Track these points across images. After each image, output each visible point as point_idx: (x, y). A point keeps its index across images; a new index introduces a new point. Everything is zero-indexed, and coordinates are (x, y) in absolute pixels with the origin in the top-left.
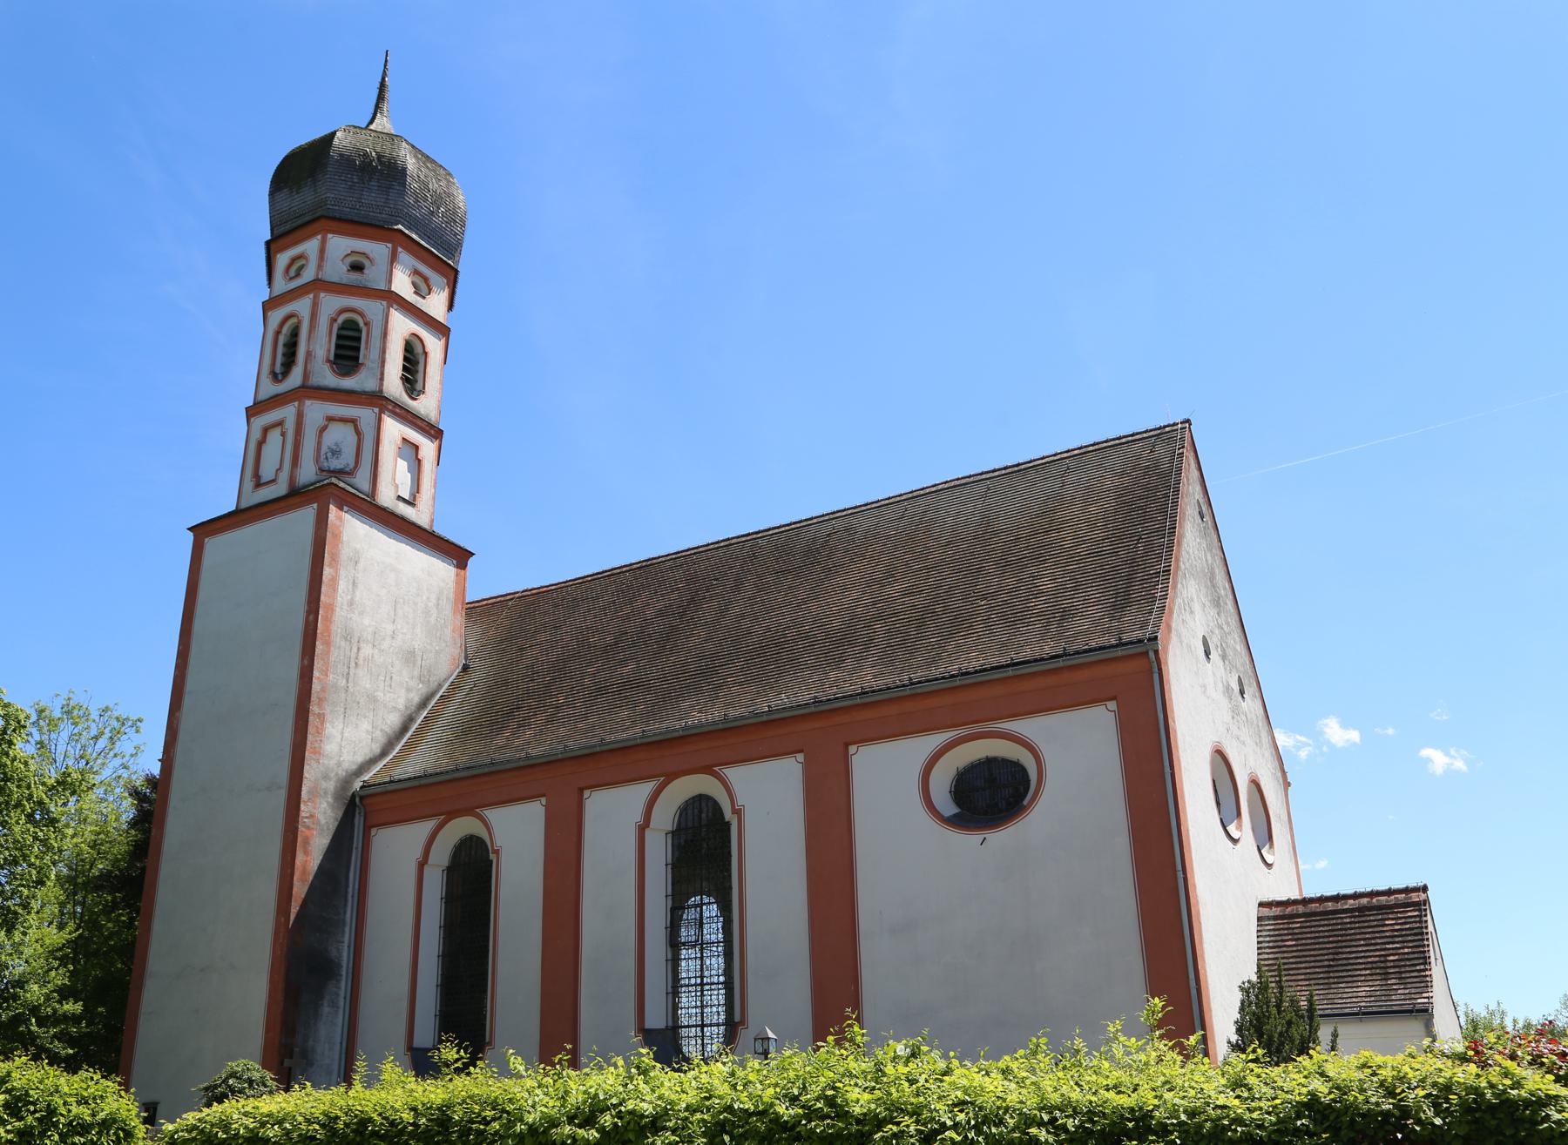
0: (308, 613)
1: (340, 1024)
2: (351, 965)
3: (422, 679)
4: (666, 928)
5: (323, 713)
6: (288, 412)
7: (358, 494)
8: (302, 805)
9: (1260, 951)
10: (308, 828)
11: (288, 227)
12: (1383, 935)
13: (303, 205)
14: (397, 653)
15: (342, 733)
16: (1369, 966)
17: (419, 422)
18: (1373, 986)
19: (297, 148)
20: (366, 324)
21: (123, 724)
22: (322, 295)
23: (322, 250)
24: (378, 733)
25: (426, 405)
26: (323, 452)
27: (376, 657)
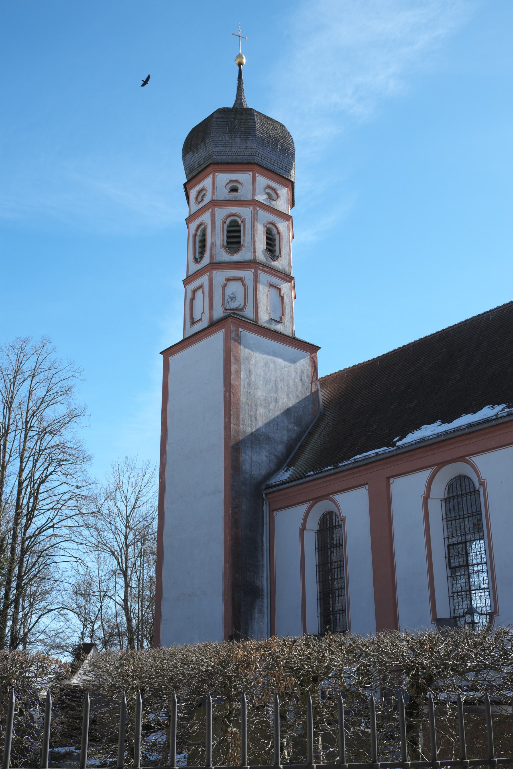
0: (225, 392)
1: (266, 623)
2: (269, 590)
4: (446, 558)
6: (204, 280)
11: (194, 173)
13: (201, 159)
20: (242, 222)
22: (216, 209)
24: (273, 457)
26: (226, 299)
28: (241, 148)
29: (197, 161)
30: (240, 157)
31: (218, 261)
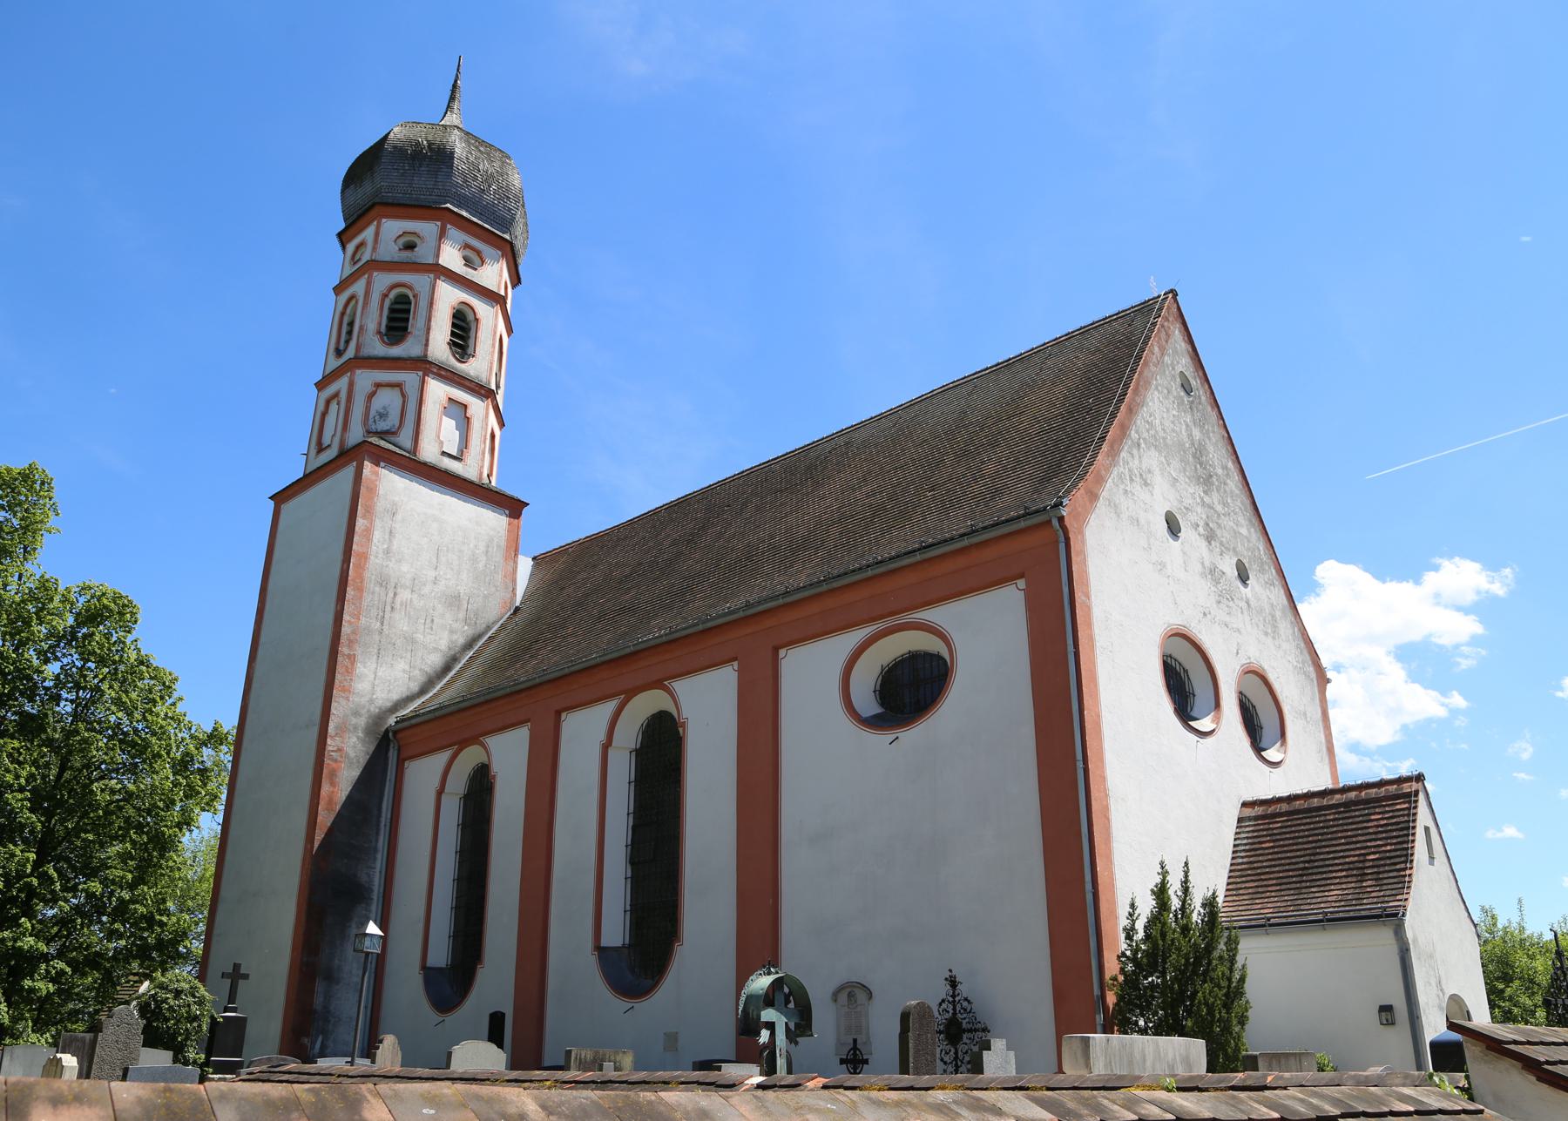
0: (344, 562)
3: (468, 621)
4: (627, 846)
5: (354, 655)
6: (342, 384)
9: (1235, 855)
10: (336, 761)
12: (1366, 831)
14: (439, 597)
15: (375, 673)
16: (1346, 867)
17: (467, 383)
18: (1345, 889)
20: (414, 296)
22: (375, 274)
24: (417, 672)
25: (478, 366)
26: (371, 416)
27: (415, 602)
28: (427, 183)
31: (366, 355)
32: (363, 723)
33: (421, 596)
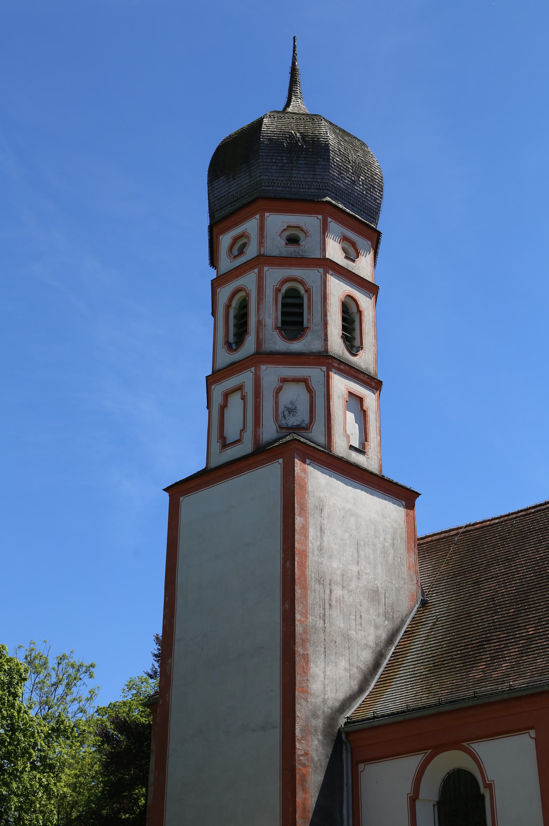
5: (307, 654)
7: (317, 447)
8: (297, 744)
10: (304, 765)
11: (227, 210)
13: (240, 189)
15: (325, 672)
17: (361, 376)
19: (227, 138)
20: (306, 291)
21: (78, 670)
22: (266, 269)
23: (262, 228)
24: (355, 670)
26: (280, 411)
27: (346, 597)
28: (306, 176)
29: (234, 192)
30: (304, 190)
32: (320, 725)
33: (350, 591)
